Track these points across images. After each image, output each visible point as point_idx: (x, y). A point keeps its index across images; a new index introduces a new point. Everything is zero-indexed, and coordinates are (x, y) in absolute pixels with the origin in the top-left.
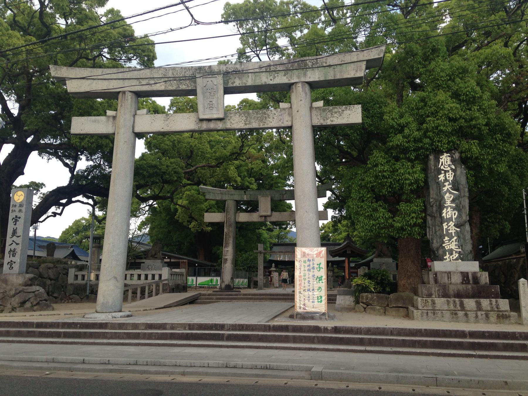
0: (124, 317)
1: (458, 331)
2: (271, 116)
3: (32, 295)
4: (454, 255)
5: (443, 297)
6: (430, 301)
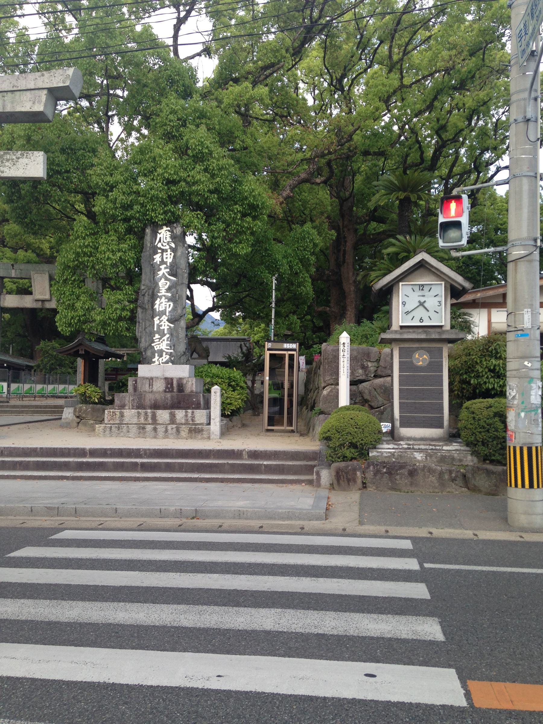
1: (78, 449)
4: (163, 358)
5: (138, 407)
6: (118, 413)
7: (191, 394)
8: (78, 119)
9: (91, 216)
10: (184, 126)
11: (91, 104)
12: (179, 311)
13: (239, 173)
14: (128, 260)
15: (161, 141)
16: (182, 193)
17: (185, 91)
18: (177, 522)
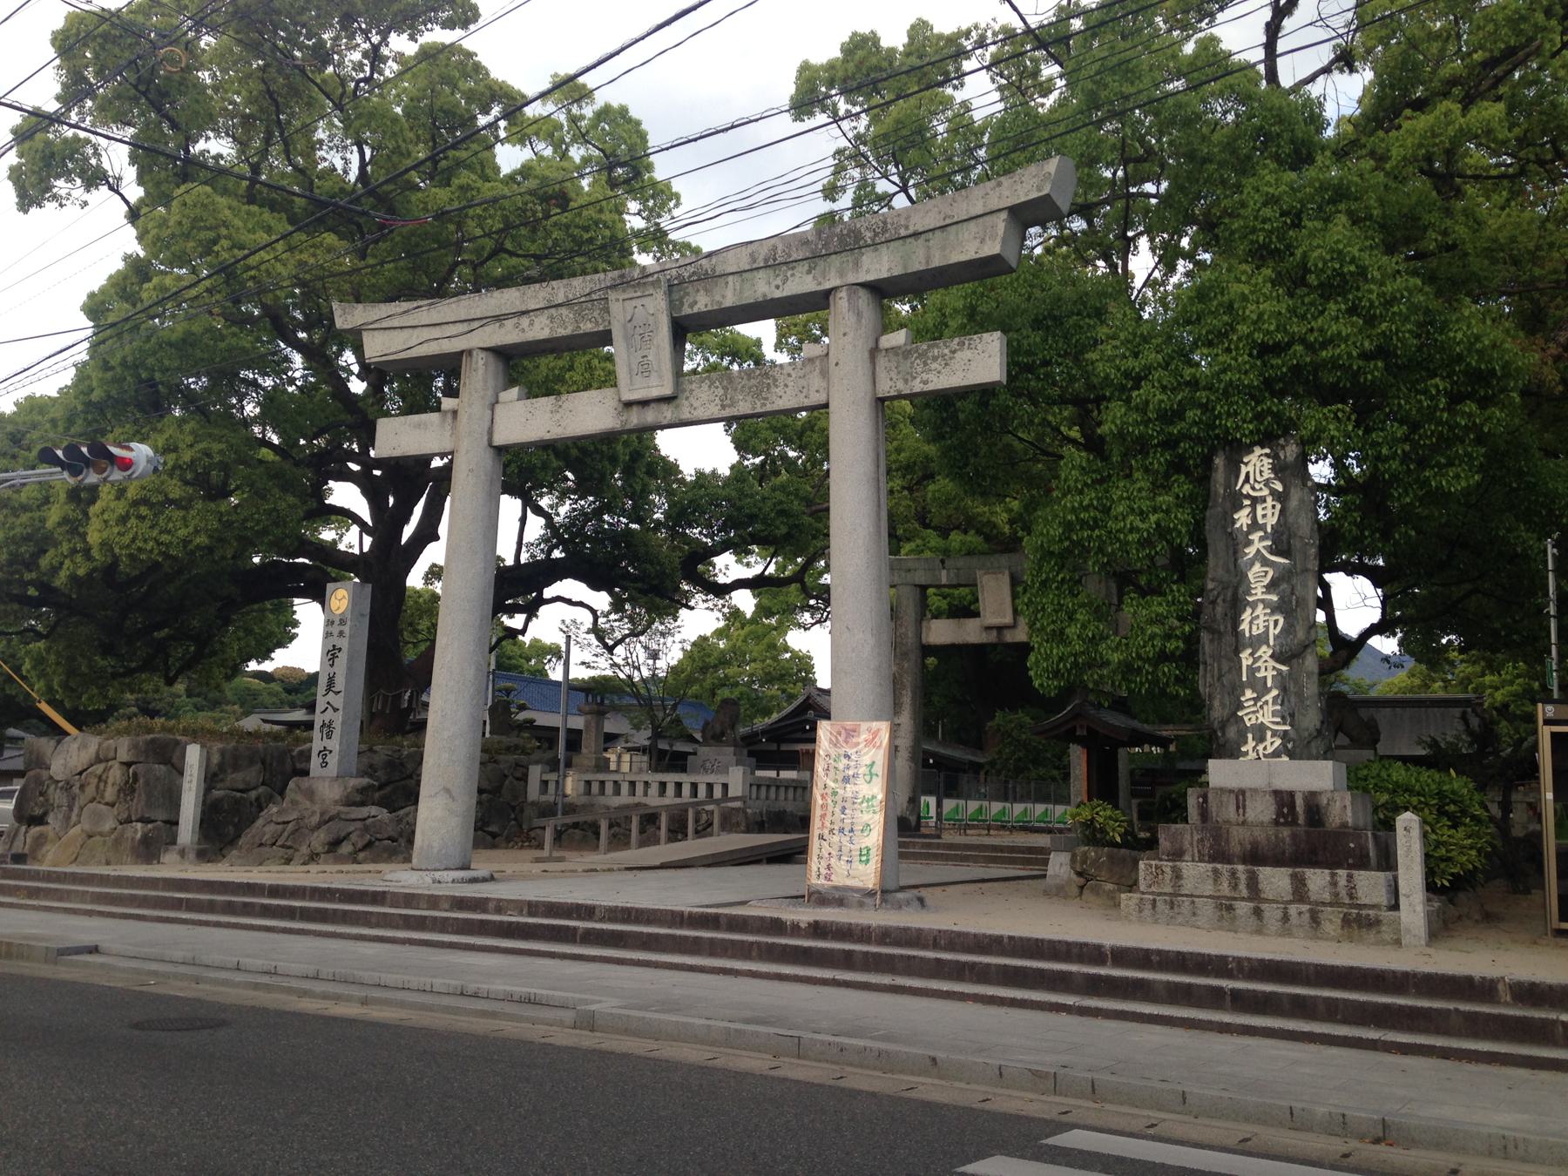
0: (463, 881)
1: (1086, 944)
2: (781, 382)
3: (359, 825)
4: (1268, 743)
6: (1168, 870)
7: (1343, 832)
8: (1065, 257)
9: (1094, 444)
10: (1297, 225)
11: (1090, 223)
12: (1301, 635)
13: (1435, 305)
14: (1175, 528)
15: (1244, 267)
16: (1297, 370)
17: (1297, 151)
18: (1337, 1146)
